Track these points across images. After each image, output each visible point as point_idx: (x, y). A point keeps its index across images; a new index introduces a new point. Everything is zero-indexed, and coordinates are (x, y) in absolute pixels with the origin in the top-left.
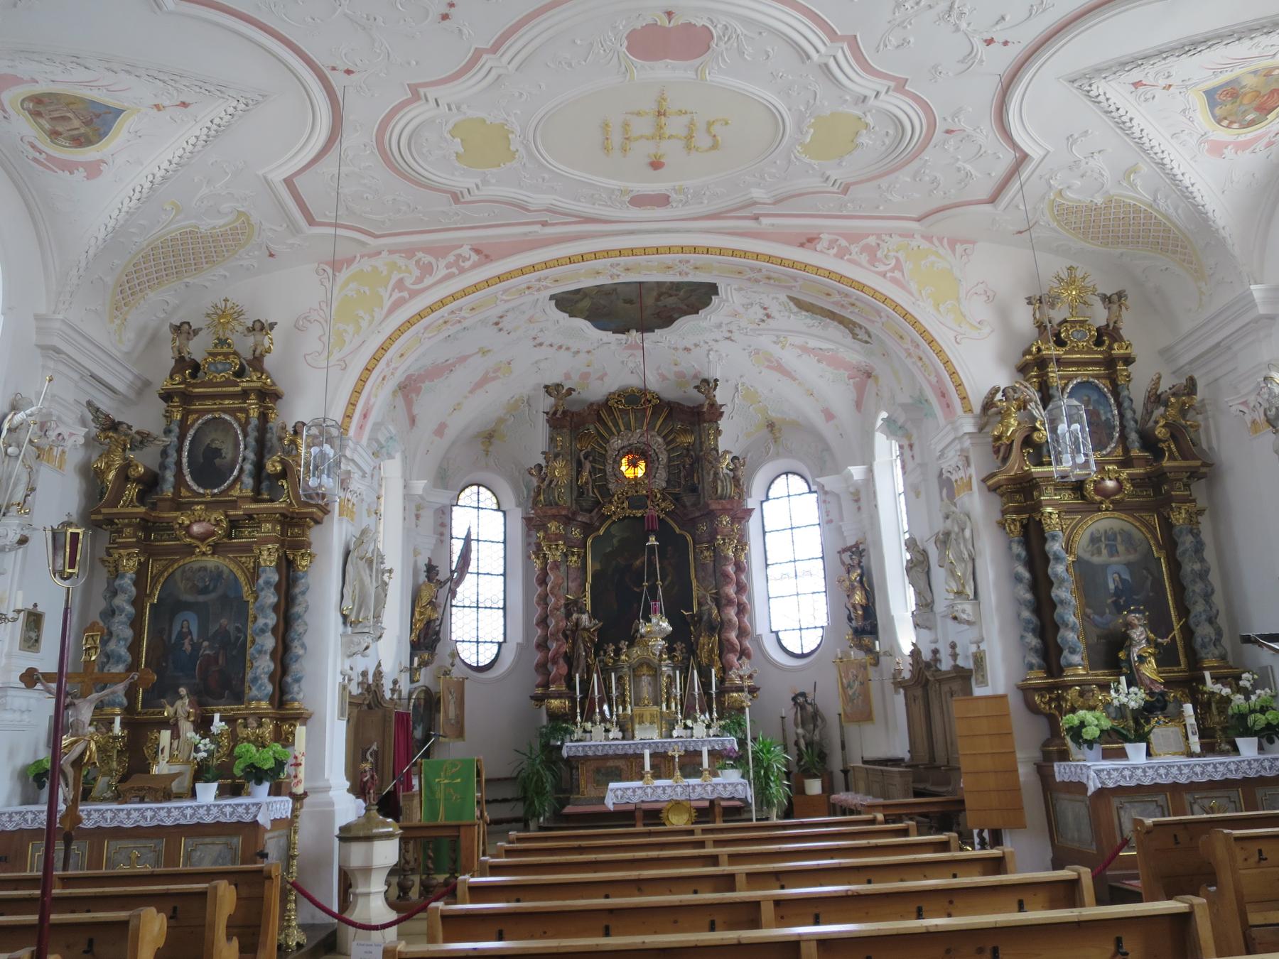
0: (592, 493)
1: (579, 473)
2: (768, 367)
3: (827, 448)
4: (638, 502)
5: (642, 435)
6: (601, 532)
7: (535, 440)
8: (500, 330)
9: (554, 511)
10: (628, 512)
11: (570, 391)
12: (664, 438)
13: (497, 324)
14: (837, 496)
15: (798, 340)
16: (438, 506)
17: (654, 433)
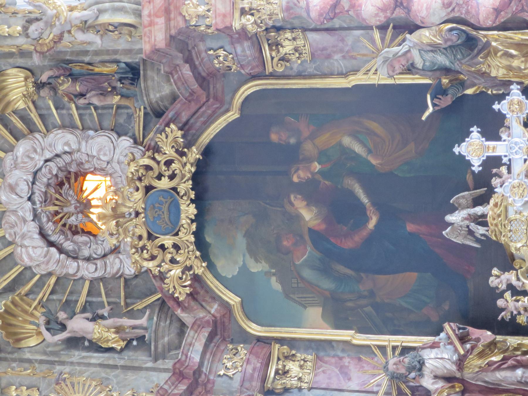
1: (95, 347)
10: (187, 237)
12: (17, 136)
17: (9, 159)
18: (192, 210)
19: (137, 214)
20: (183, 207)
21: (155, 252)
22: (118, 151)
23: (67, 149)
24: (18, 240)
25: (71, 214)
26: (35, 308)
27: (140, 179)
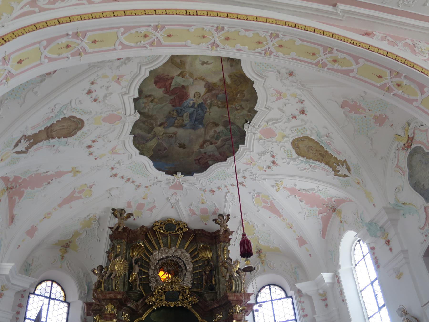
0: (139, 289)
1: (130, 273)
2: (264, 207)
3: (299, 265)
4: (172, 296)
5: (176, 251)
6: (144, 317)
7: (98, 251)
8: (91, 154)
9: (112, 296)
10: (164, 303)
11: (129, 215)
12: (191, 254)
13: (90, 147)
14: (309, 297)
15: (289, 183)
16: (19, 289)
17: (184, 250)
18: (172, 306)
19: (172, 288)
20: (173, 303)
21: (160, 294)
22: (187, 283)
23: (188, 268)
24: (160, 251)
25: (167, 268)
26: (140, 255)
27: (182, 290)
